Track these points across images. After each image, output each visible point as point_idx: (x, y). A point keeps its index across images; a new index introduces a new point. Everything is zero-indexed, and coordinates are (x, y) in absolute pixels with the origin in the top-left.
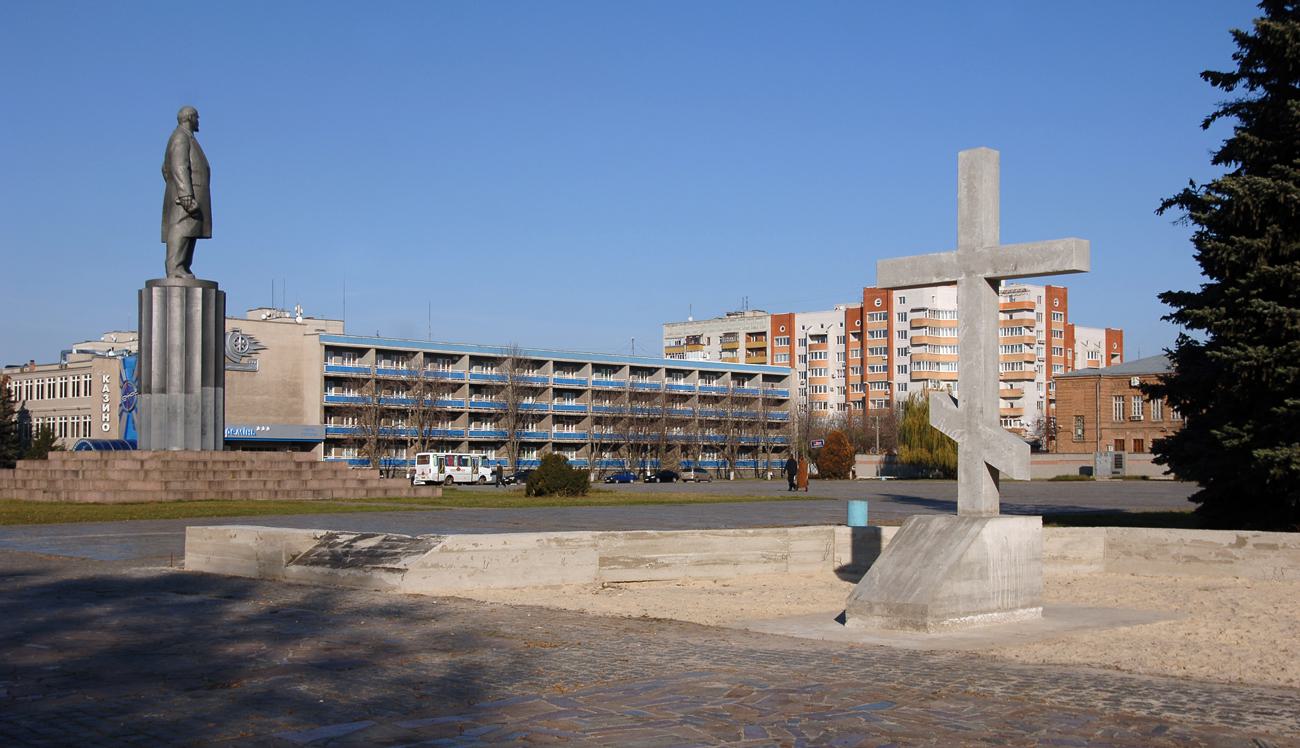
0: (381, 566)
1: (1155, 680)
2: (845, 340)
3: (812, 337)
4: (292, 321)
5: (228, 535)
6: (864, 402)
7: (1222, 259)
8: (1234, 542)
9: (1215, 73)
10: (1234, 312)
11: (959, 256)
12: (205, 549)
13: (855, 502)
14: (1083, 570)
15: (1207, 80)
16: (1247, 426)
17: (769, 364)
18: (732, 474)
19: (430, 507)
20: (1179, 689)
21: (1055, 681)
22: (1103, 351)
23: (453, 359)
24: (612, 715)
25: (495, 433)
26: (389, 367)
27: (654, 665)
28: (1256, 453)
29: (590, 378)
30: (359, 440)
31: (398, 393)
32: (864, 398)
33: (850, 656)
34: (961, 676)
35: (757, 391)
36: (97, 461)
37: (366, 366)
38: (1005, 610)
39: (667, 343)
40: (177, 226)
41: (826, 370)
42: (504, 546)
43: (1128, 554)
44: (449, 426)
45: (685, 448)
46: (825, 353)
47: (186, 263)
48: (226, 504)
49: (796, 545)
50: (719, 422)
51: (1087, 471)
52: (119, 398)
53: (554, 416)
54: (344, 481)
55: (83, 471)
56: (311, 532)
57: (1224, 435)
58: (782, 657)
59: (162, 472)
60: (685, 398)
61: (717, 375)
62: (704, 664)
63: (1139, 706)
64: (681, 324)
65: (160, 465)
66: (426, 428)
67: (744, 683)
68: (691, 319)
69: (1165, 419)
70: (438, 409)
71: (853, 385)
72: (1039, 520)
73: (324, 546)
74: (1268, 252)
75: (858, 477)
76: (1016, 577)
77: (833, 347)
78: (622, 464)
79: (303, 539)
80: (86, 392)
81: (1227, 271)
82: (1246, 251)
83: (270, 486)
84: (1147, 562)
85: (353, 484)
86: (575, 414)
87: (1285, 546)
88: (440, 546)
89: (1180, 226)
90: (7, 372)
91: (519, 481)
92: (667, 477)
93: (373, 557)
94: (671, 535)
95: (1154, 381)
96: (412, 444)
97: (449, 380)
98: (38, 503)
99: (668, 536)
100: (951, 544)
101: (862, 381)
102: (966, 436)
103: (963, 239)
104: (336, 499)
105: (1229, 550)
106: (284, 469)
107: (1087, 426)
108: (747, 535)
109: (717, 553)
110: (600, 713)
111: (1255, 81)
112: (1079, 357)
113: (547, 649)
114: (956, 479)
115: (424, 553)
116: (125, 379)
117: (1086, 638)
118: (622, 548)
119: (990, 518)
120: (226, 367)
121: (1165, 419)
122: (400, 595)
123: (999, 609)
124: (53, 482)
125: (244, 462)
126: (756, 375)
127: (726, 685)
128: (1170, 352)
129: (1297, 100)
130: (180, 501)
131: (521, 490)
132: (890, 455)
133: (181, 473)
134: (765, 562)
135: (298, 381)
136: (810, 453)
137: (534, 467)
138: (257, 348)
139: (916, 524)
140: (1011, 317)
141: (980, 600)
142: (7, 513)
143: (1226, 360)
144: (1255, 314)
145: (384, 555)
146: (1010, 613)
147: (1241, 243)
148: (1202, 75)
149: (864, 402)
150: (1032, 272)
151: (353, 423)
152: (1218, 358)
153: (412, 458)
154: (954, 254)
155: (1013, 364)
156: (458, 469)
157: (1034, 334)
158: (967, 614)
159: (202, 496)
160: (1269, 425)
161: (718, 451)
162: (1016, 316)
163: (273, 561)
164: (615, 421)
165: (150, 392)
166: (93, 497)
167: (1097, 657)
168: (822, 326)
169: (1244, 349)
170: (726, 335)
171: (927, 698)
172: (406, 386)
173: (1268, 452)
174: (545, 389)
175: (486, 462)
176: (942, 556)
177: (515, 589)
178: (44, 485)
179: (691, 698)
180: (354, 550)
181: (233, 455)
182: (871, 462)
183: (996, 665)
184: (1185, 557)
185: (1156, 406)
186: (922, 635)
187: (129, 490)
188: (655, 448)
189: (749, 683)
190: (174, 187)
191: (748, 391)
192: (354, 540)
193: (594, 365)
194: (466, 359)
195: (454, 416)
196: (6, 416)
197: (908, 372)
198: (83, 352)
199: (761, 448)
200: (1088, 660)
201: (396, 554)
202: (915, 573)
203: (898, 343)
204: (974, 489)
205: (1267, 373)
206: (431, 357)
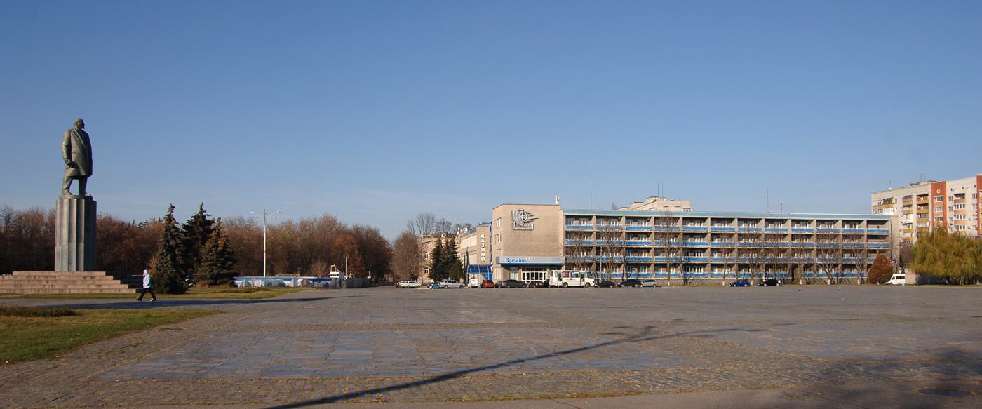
3: (956, 195)
41: (964, 216)
46: (964, 205)
68: (890, 189)
77: (970, 200)
135: (556, 234)
156: (571, 279)
168: (963, 188)
170: (906, 197)
194: (763, 221)
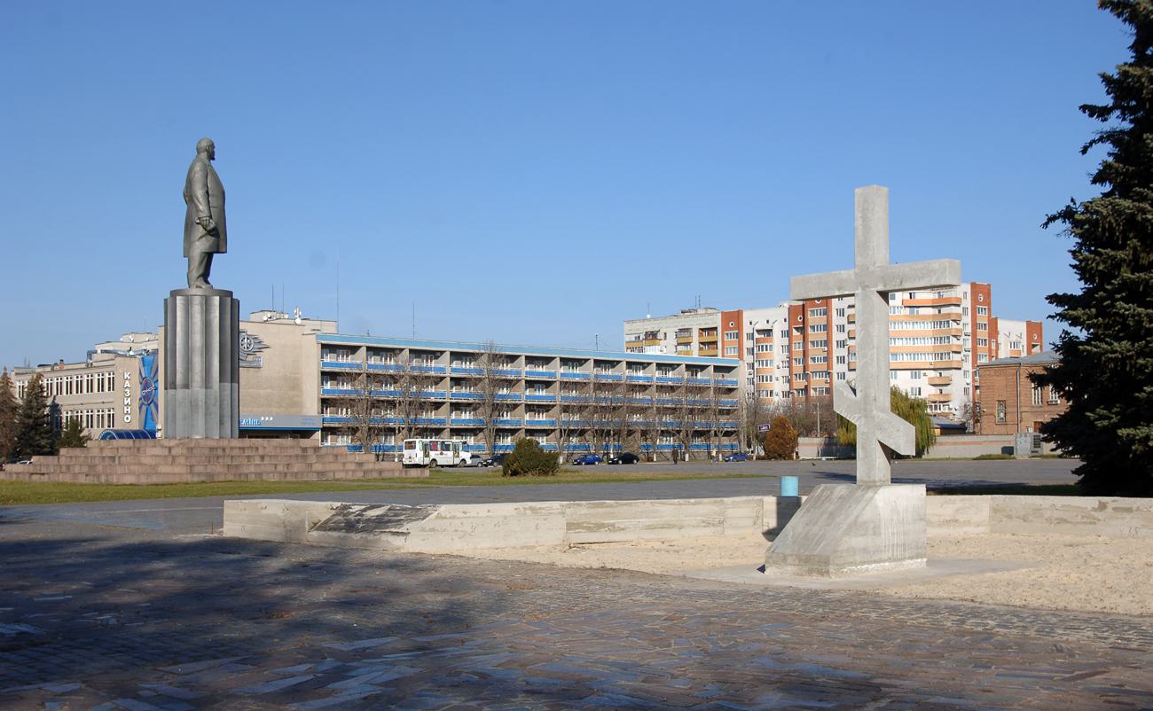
0: (387, 530)
1: (997, 608)
2: (788, 334)
3: (758, 331)
4: (292, 322)
5: (259, 507)
6: (806, 389)
7: (1092, 268)
8: (1096, 507)
9: (1091, 106)
10: (1102, 312)
11: (855, 273)
12: (242, 519)
13: (787, 477)
14: (972, 531)
15: (1084, 112)
16: (1115, 410)
17: (720, 357)
18: (687, 456)
19: (419, 485)
20: (1016, 613)
21: (920, 609)
22: (1024, 341)
23: (435, 355)
24: (575, 632)
25: (474, 421)
26: (378, 363)
27: (609, 600)
28: (1120, 432)
29: (558, 371)
30: (353, 429)
31: (386, 385)
32: (806, 387)
33: (764, 593)
34: (848, 606)
35: (709, 381)
36: (130, 448)
37: (358, 362)
38: (895, 560)
39: (627, 338)
40: (197, 243)
41: (771, 361)
42: (488, 514)
43: (1010, 517)
44: (432, 415)
45: (644, 433)
46: (771, 346)
47: (205, 275)
48: (244, 485)
49: (731, 512)
50: (674, 409)
51: (1008, 451)
52: (138, 393)
53: (527, 405)
54: (344, 464)
55: (119, 457)
56: (329, 503)
57: (1097, 416)
58: (711, 595)
59: (187, 458)
60: (644, 388)
61: (673, 367)
62: (649, 600)
63: (978, 625)
64: (640, 321)
65: (185, 451)
66: (412, 417)
67: (677, 612)
68: (648, 316)
69: (1055, 404)
70: (423, 400)
71: (796, 375)
72: (922, 488)
73: (340, 515)
74: (1131, 261)
75: (801, 458)
76: (904, 534)
77: (778, 340)
78: (588, 448)
79: (322, 509)
80: (109, 388)
81: (1097, 278)
82: (1112, 261)
83: (280, 468)
84: (1025, 523)
85: (352, 467)
86: (545, 403)
87: (1138, 509)
88: (436, 513)
89: (1063, 238)
90: (39, 370)
91: (495, 464)
92: (628, 459)
93: (380, 523)
94: (626, 504)
95: (1040, 371)
96: (399, 432)
97: (432, 373)
98: (82, 485)
99: (622, 505)
100: (850, 507)
101: (804, 372)
102: (863, 420)
103: (859, 260)
104: (338, 480)
105: (1093, 513)
106: (292, 454)
107: (1009, 410)
108: (690, 504)
109: (664, 519)
110: (567, 631)
111: (1125, 111)
112: (1002, 347)
113: (525, 591)
114: (855, 458)
115: (423, 519)
116: (144, 376)
117: (956, 580)
118: (586, 515)
119: (881, 486)
120: (241, 364)
121: (1055, 404)
122: (404, 553)
123: (890, 560)
124: (92, 467)
125: (257, 448)
126: (708, 366)
127: (664, 613)
128: (1057, 346)
129: (1151, 133)
130: (203, 482)
131: (498, 471)
132: (830, 437)
133: (204, 458)
134: (705, 527)
136: (757, 437)
137: (508, 451)
138: (262, 347)
139: (823, 491)
140: (939, 311)
141: (874, 552)
142: (60, 493)
143: (1096, 353)
144: (1117, 314)
145: (390, 521)
146: (899, 563)
147: (1107, 254)
148: (1080, 108)
149: (806, 389)
150: (915, 286)
151: (341, 413)
152: (1088, 351)
153: (400, 444)
154: (852, 272)
155: (942, 354)
156: (441, 454)
157: (961, 327)
158: (863, 563)
159: (222, 478)
160: (1134, 409)
161: (674, 435)
162: (944, 310)
163: (298, 527)
164: (581, 409)
165: (175, 388)
166: (129, 479)
167: (959, 593)
168: (768, 322)
169: (1110, 344)
170: (681, 330)
171: (816, 620)
172: (394, 379)
173: (1131, 431)
174: (518, 381)
175: (466, 447)
176: (842, 517)
177: (497, 549)
178: (85, 469)
179: (636, 621)
180: (364, 518)
181: (247, 442)
182: (812, 444)
183: (877, 599)
184: (1057, 519)
185: (1050, 393)
186: (825, 579)
187: (160, 474)
188: (618, 433)
189: (681, 612)
190: (194, 209)
191: (701, 381)
192: (365, 510)
193: (562, 359)
194: (447, 355)
195: (437, 406)
196: (39, 409)
197: (846, 362)
198: (106, 352)
199: (713, 432)
200: (951, 596)
201: (400, 520)
202: (820, 530)
203: (837, 336)
204: (871, 462)
205: (1131, 364)
206: (416, 353)
